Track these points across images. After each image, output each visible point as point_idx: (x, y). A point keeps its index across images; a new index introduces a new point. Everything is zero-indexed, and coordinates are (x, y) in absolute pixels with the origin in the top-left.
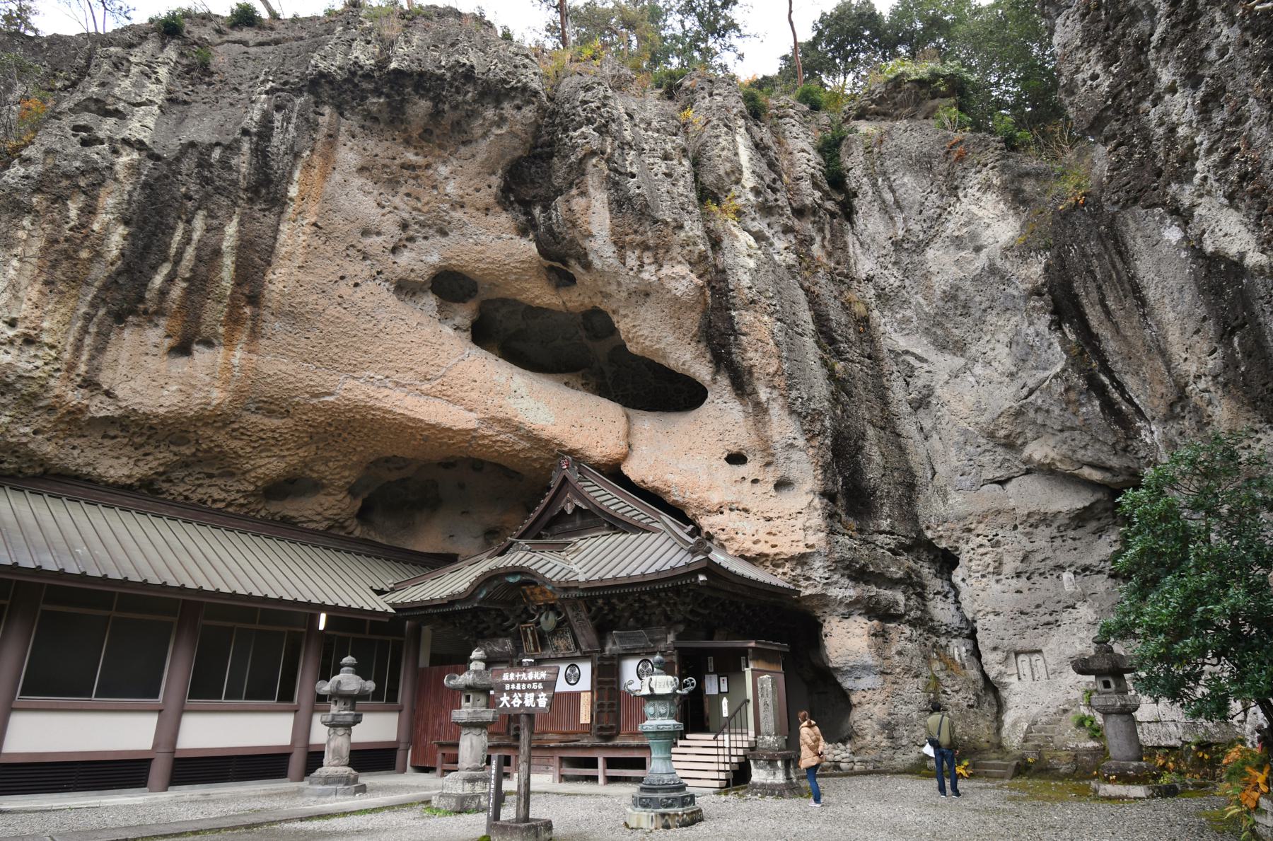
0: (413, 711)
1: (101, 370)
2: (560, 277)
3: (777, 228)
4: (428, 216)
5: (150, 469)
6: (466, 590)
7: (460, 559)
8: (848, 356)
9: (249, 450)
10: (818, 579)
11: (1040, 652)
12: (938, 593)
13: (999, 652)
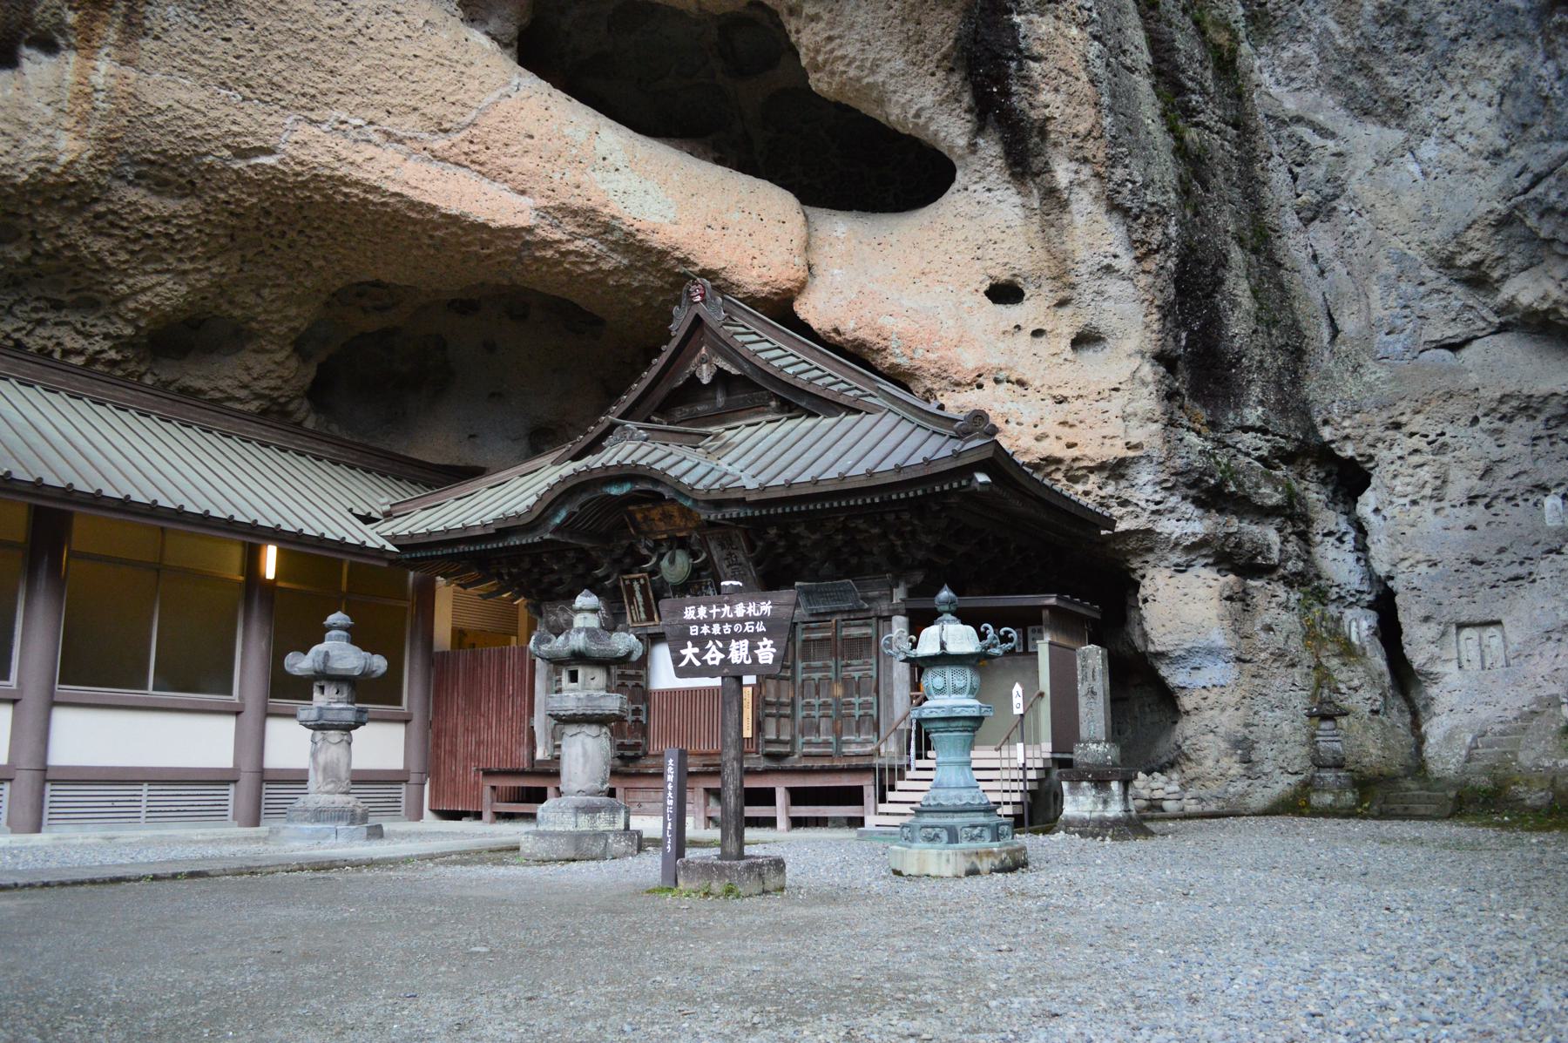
0: (428, 724)
6: (530, 510)
8: (1202, 117)
9: (123, 256)
10: (1143, 504)
11: (1498, 623)
12: (1330, 534)
13: (1432, 625)
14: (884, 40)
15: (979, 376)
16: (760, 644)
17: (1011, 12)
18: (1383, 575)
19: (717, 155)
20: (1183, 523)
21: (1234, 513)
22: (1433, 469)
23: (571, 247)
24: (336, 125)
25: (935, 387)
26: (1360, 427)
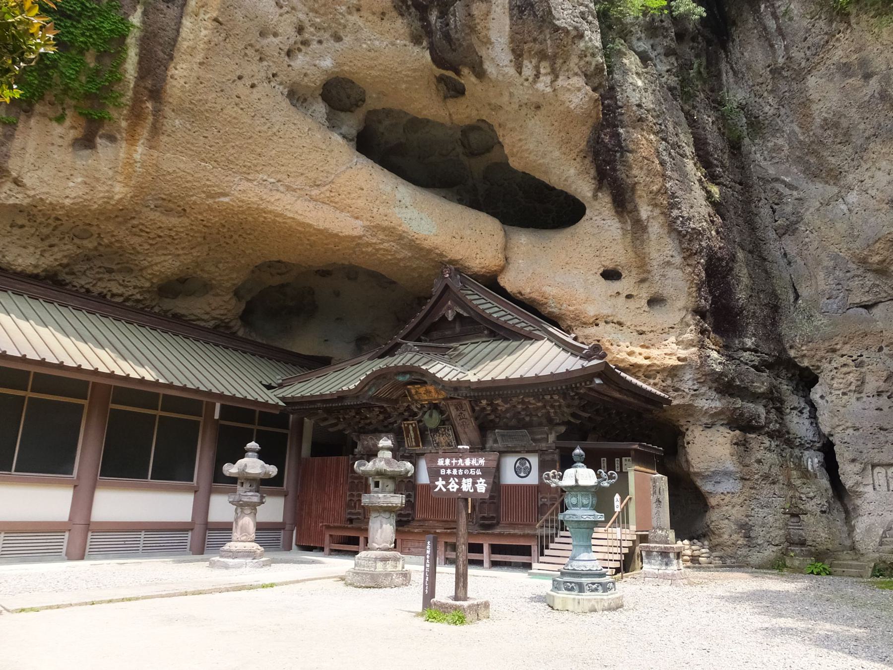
1: (9, 157)
2: (448, 89)
3: (660, 50)
4: (324, 18)
5: (56, 260)
7: (333, 361)
8: (722, 180)
9: (147, 246)
10: (687, 390)
12: (794, 408)
14: (549, 141)
15: (597, 319)
16: (478, 481)
17: (618, 127)
18: (826, 433)
19: (459, 197)
20: (709, 401)
21: (738, 396)
22: (856, 375)
23: (382, 247)
24: (261, 182)
25: (573, 324)
26: (812, 350)
